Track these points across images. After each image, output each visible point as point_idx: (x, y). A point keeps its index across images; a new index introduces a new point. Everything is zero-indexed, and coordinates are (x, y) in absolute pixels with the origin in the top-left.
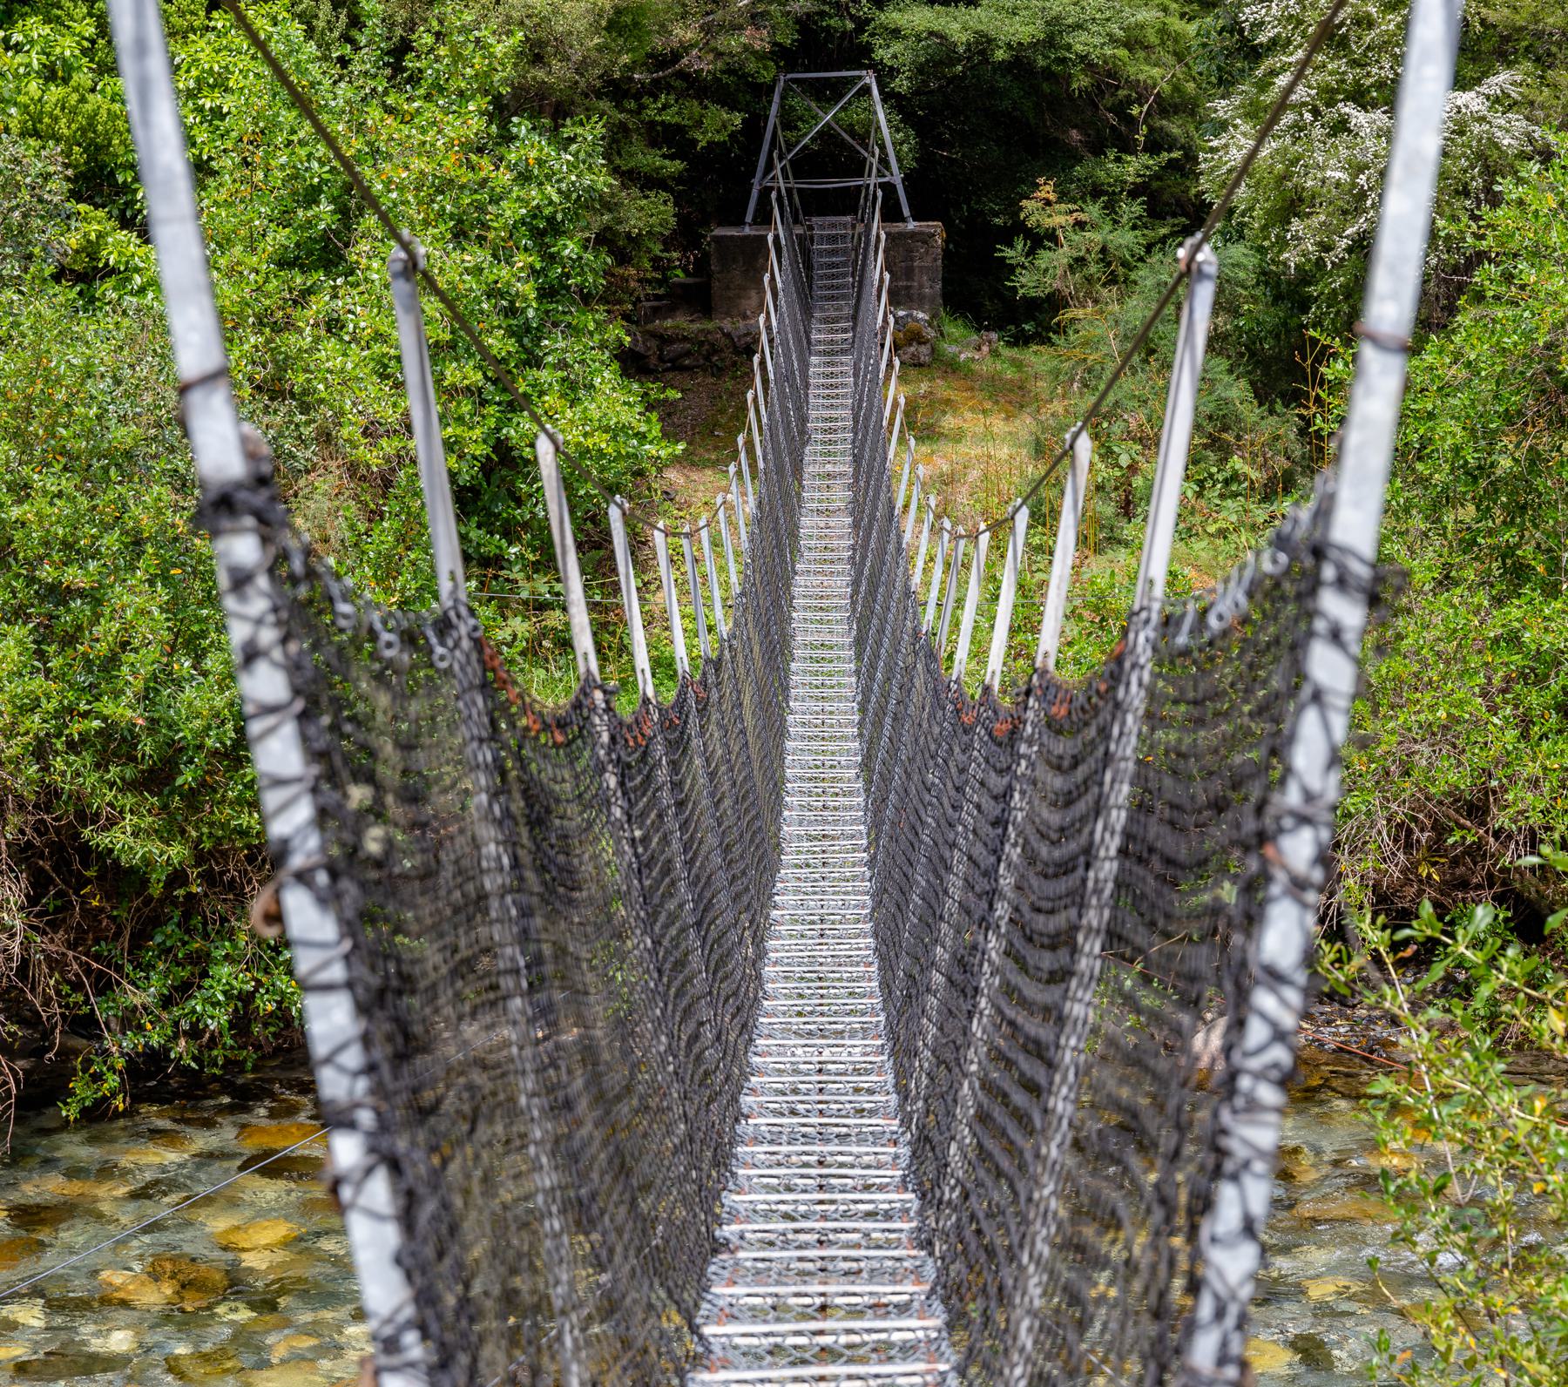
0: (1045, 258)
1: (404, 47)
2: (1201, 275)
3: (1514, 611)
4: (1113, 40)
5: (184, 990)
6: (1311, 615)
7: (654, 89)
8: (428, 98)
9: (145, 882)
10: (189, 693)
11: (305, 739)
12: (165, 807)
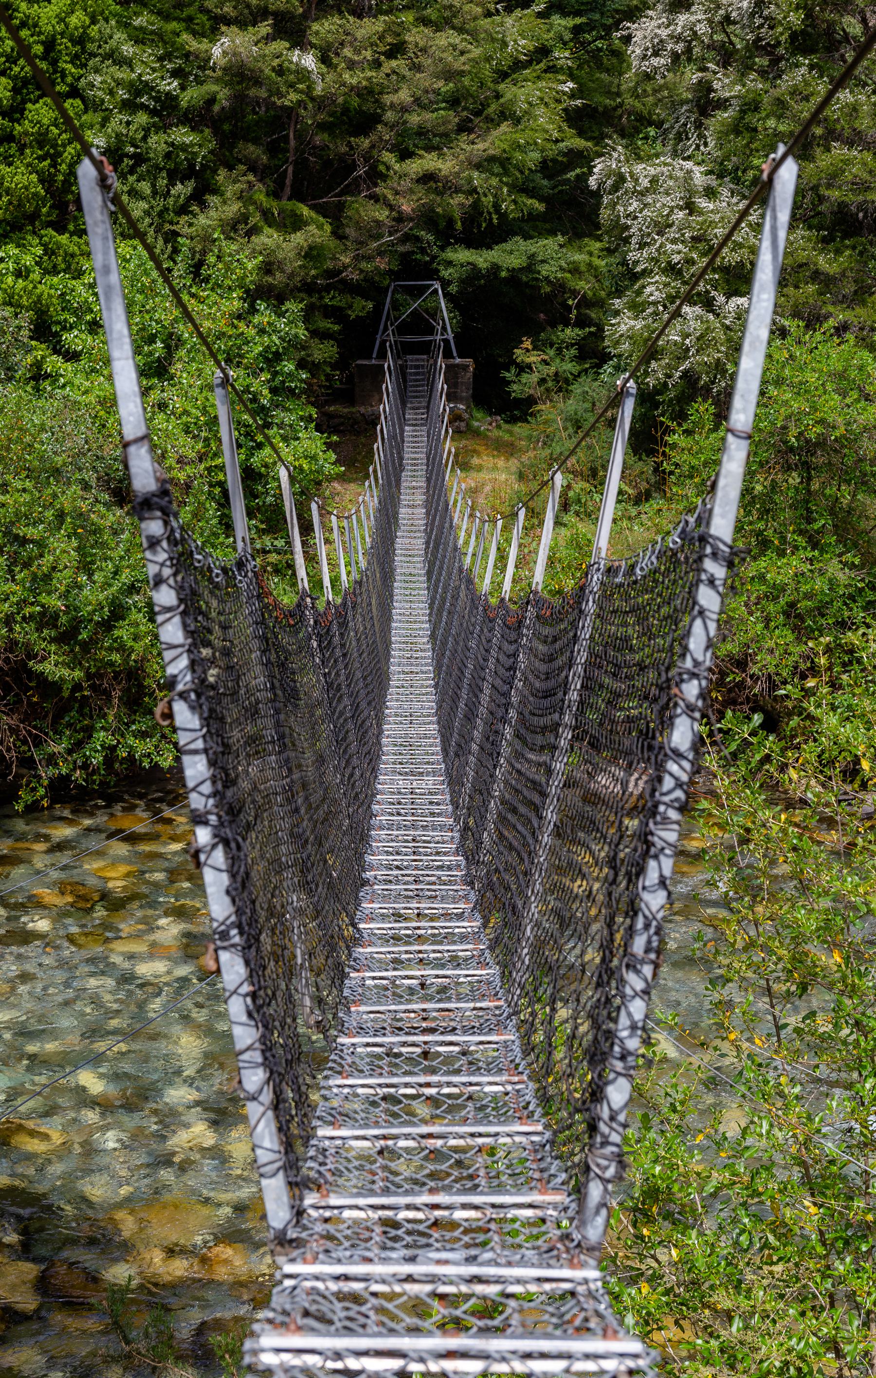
0: (525, 377)
1: (199, 265)
2: (629, 394)
3: (762, 563)
4: (562, 269)
5: (78, 746)
6: (700, 570)
7: (327, 288)
8: (212, 289)
9: (60, 689)
10: (86, 592)
11: (185, 626)
12: (72, 651)
